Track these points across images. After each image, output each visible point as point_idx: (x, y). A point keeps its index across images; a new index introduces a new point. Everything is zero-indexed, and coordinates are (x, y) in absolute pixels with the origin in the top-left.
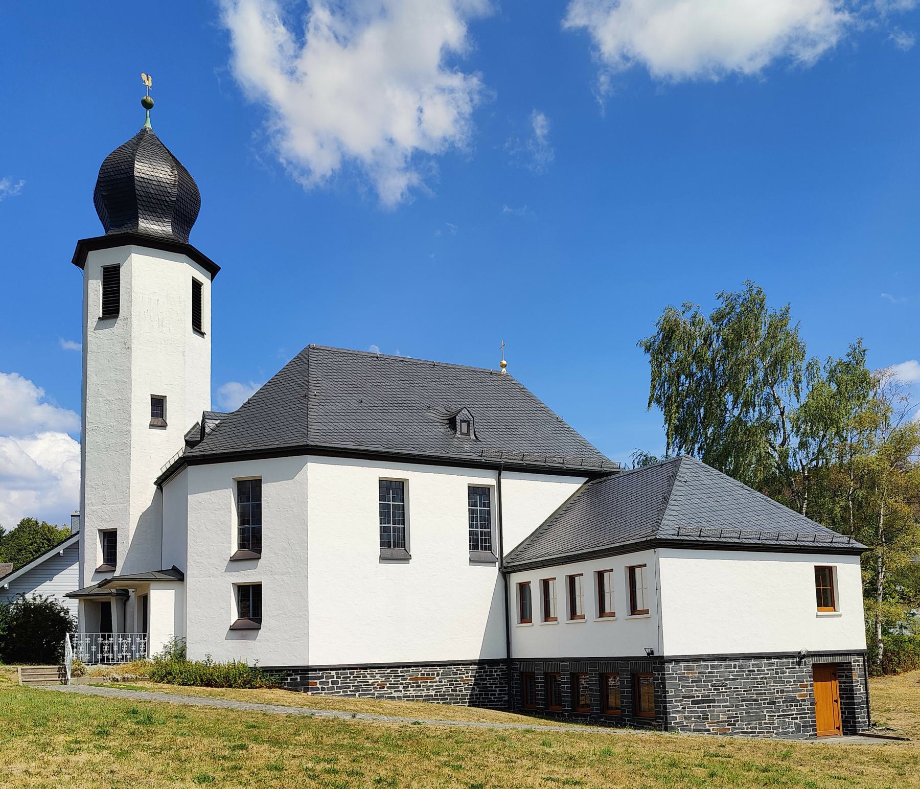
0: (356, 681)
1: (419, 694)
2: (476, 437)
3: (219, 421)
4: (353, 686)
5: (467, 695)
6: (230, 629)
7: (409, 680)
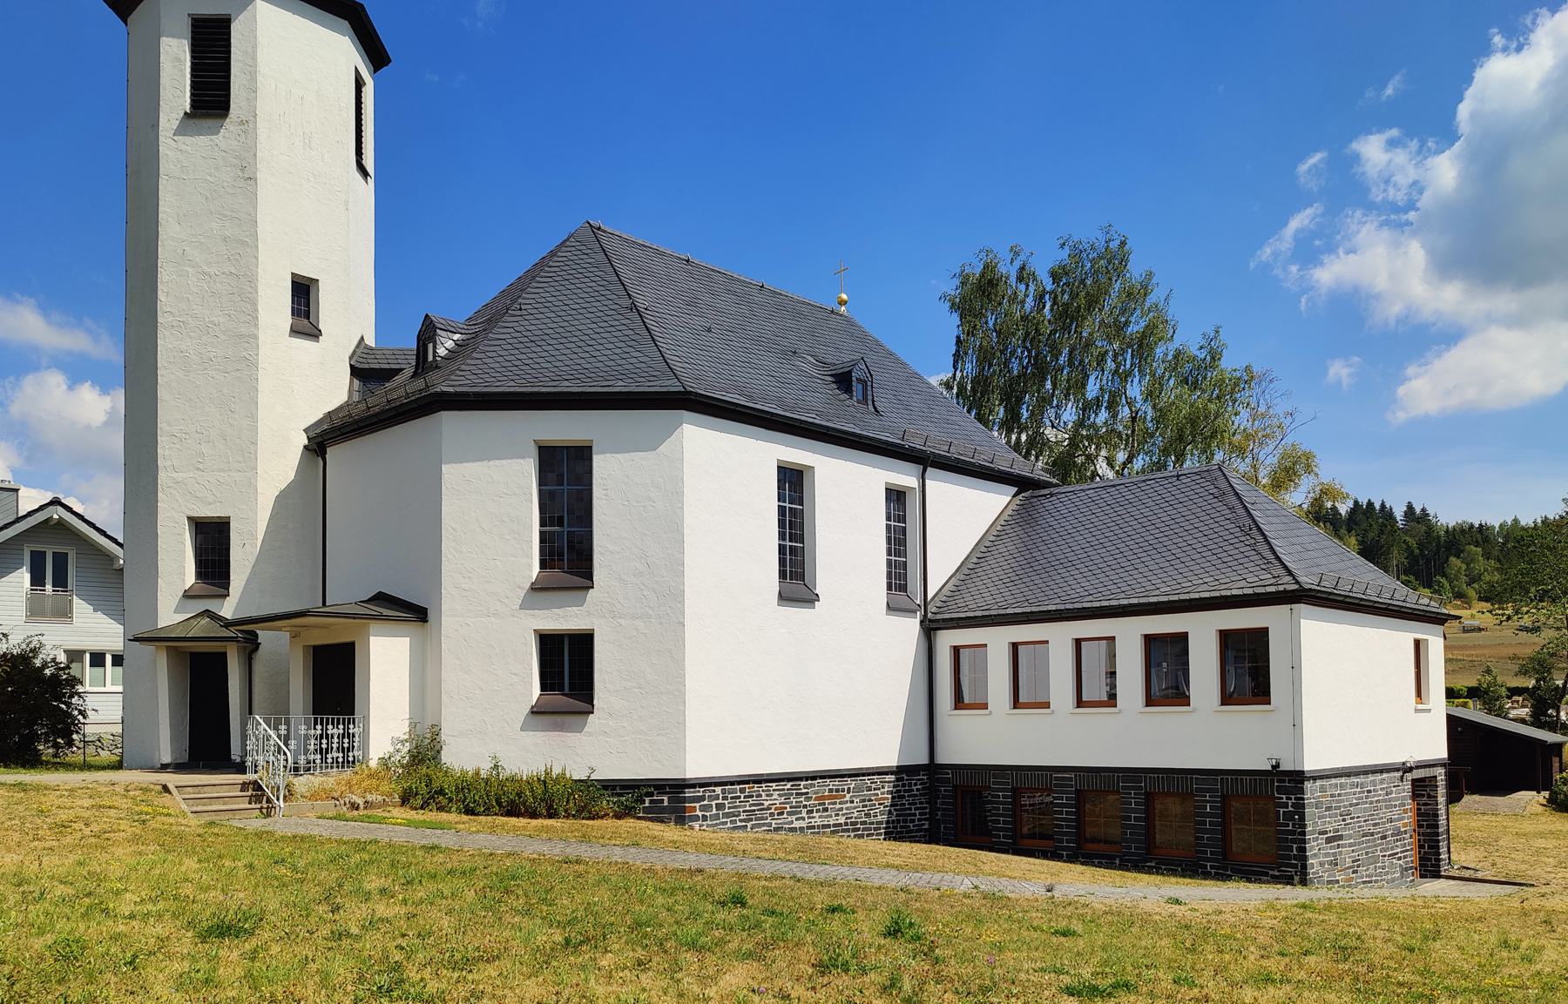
0: (748, 804)
1: (826, 823)
2: (875, 408)
3: (459, 335)
4: (744, 811)
5: (881, 823)
6: (532, 712)
7: (815, 800)
